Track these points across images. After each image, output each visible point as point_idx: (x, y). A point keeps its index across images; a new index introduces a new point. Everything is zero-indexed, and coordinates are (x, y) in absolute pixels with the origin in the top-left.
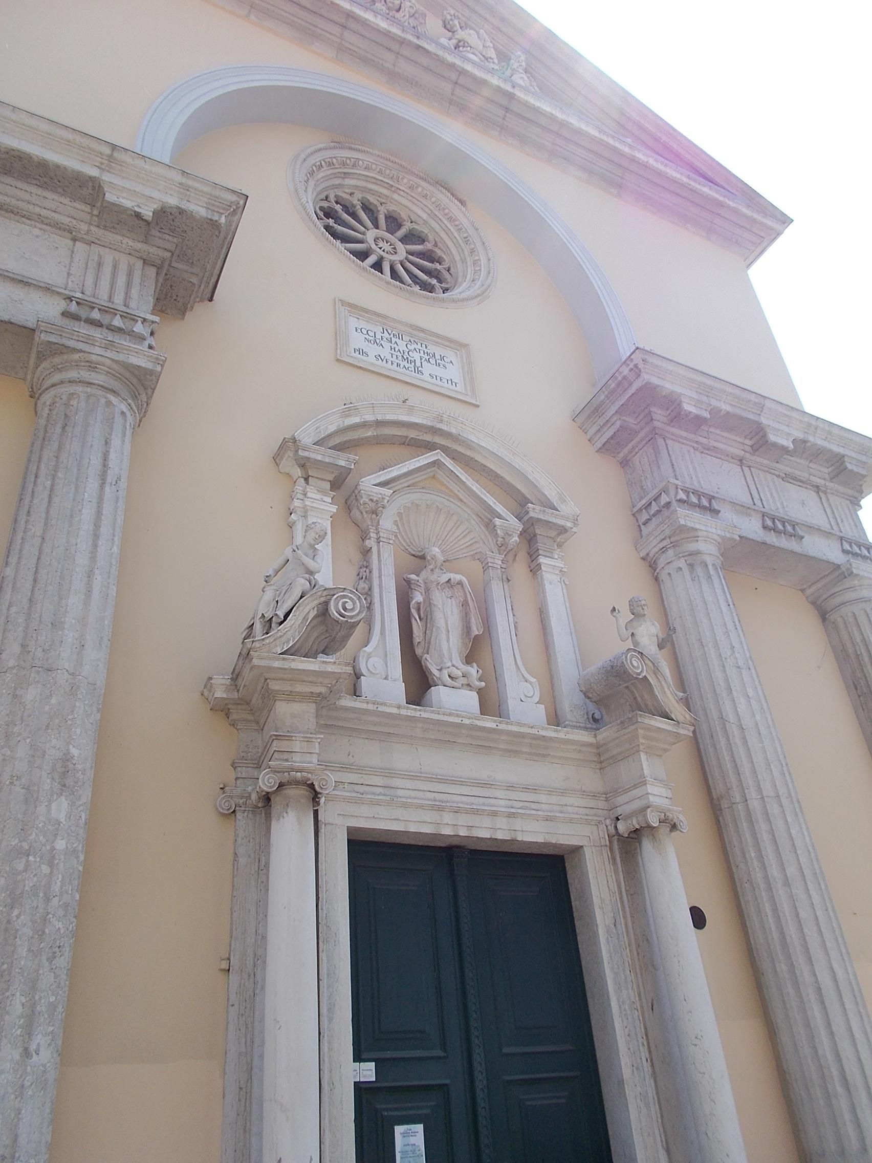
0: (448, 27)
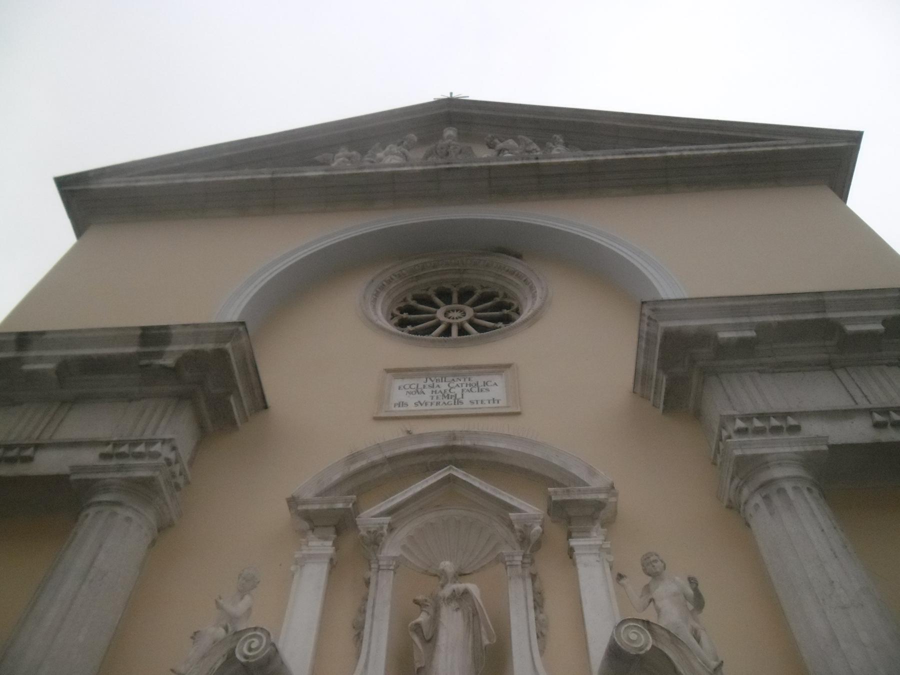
0: (491, 146)
